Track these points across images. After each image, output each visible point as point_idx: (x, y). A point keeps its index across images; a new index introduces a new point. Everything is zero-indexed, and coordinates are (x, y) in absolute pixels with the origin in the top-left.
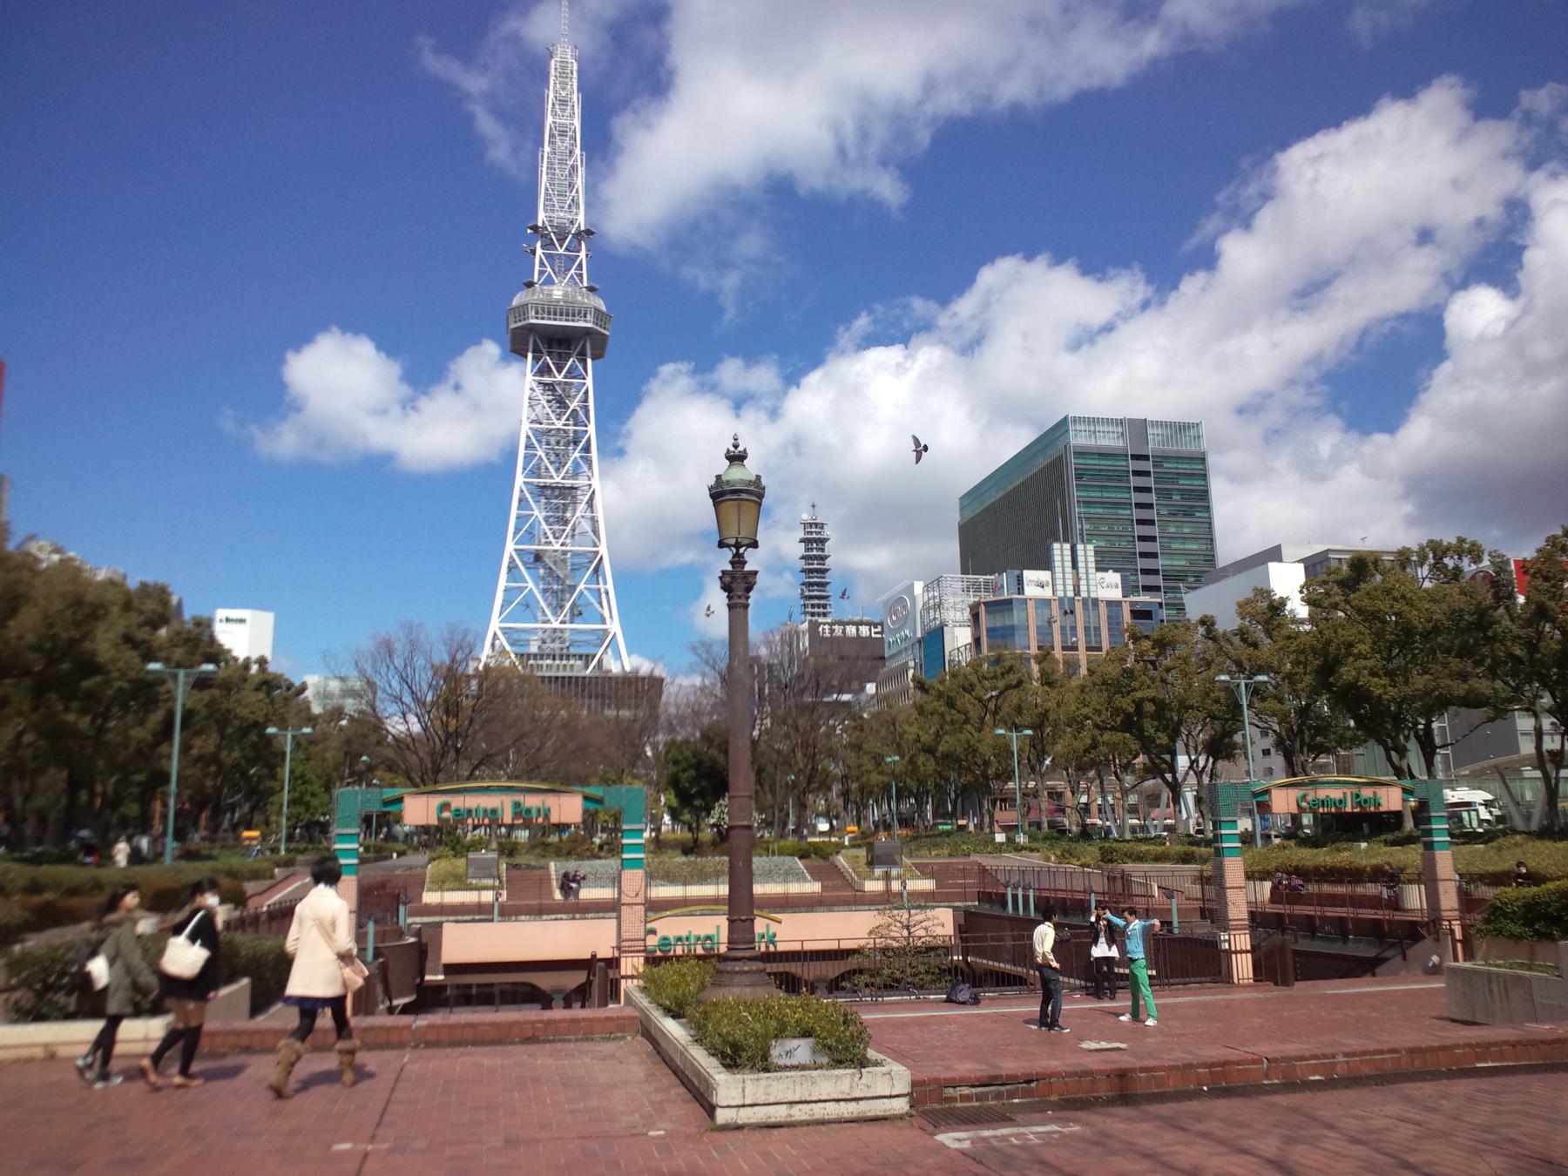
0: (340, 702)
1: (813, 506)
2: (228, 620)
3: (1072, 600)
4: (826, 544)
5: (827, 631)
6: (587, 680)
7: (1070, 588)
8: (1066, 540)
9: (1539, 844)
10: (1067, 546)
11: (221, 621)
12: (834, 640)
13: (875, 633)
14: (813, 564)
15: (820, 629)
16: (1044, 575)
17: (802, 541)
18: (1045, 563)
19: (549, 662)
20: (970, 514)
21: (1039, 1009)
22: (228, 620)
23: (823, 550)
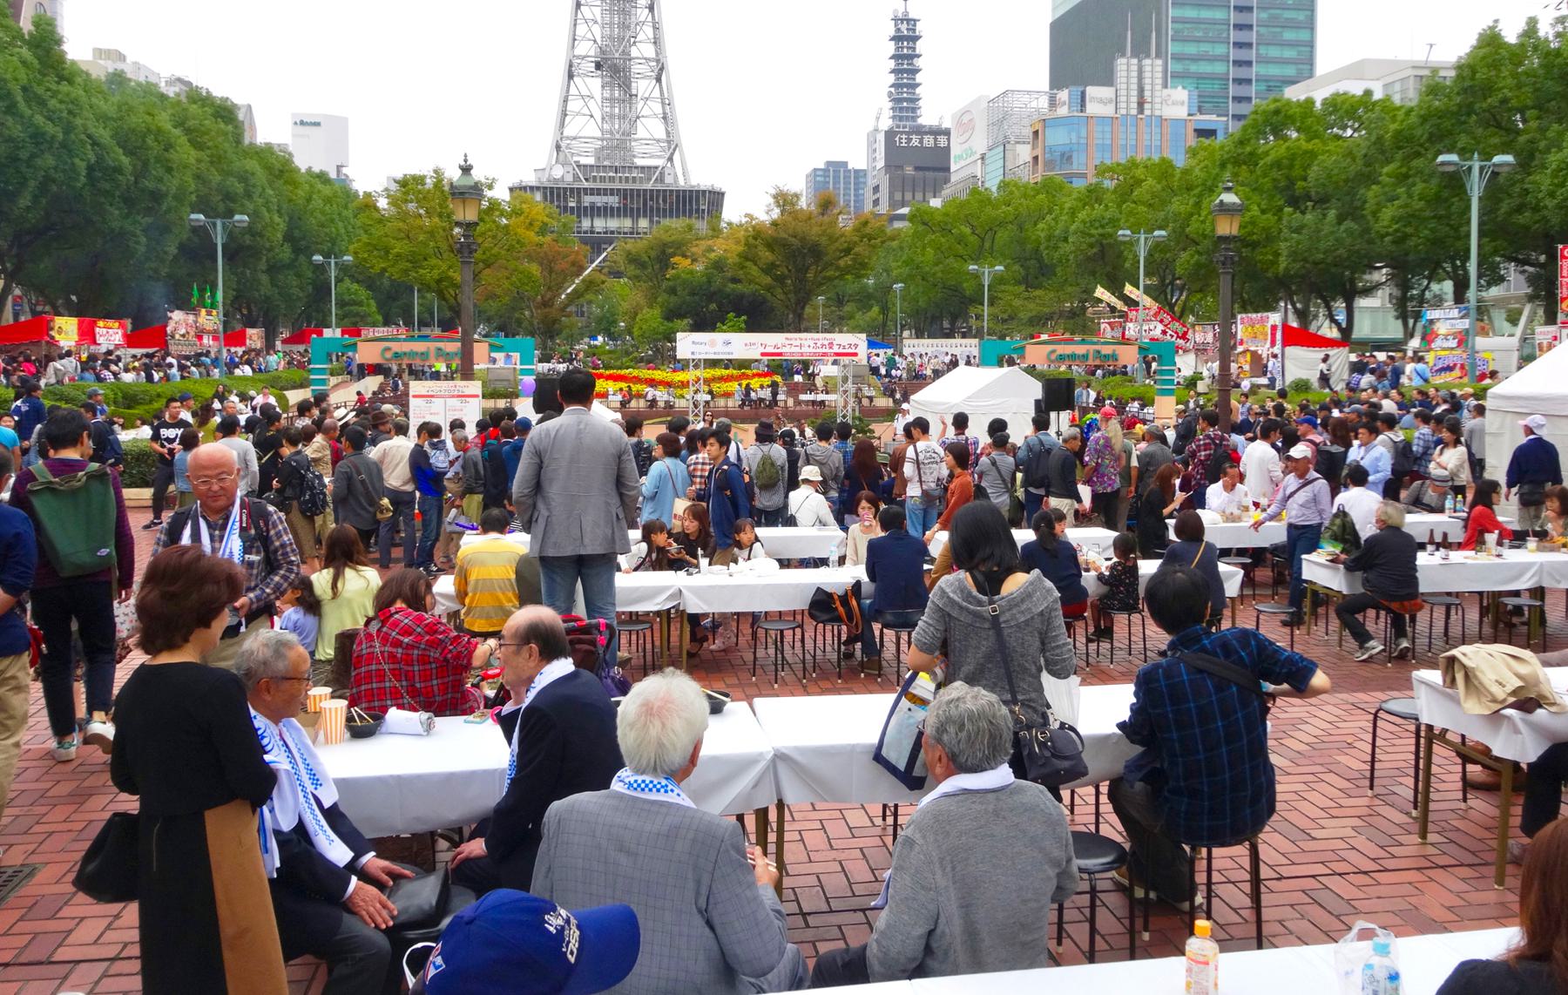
0: (1269, 562)
8: (1158, 56)
10: (1159, 62)
16: (1105, 92)
17: (893, 39)
18: (1108, 79)
20: (276, 149)
21: (476, 367)
23: (914, 49)
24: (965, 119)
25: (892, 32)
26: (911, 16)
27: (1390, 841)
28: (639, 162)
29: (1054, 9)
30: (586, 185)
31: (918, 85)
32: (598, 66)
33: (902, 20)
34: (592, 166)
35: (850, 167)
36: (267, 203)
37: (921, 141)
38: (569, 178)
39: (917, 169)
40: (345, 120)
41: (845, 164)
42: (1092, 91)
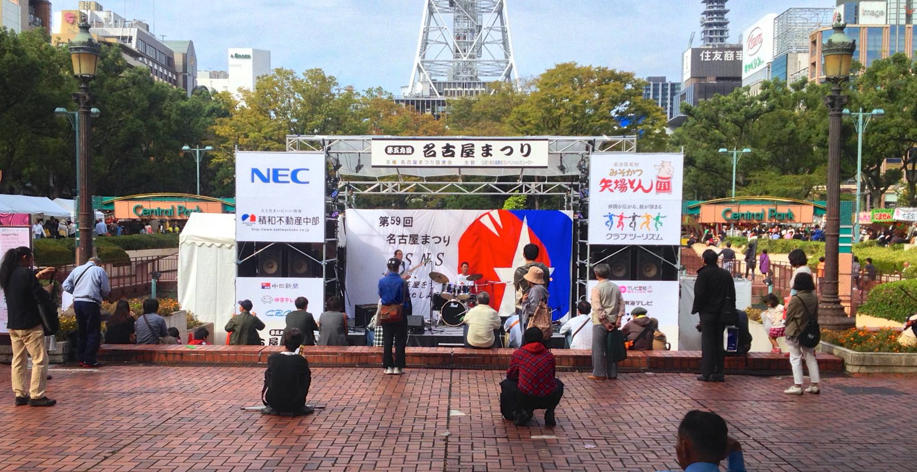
2: (237, 56)
3: (902, 28)
7: (903, 16)
11: (232, 56)
12: (712, 63)
15: (702, 55)
19: (459, 89)
21: (696, 279)
22: (237, 56)
28: (483, 79)
30: (439, 98)
34: (444, 83)
35: (667, 81)
37: (722, 57)
38: (427, 93)
39: (718, 79)
40: (270, 52)
41: (663, 79)
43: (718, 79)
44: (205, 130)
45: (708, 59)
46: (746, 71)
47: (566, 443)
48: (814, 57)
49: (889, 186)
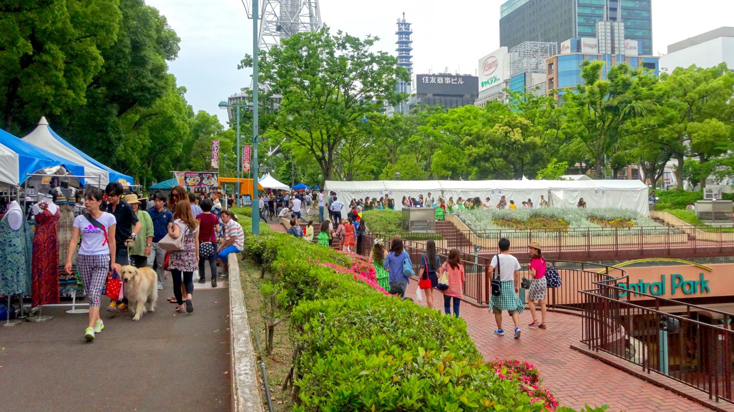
1: (404, 14)
4: (410, 36)
5: (427, 80)
6: (645, 14)
9: (460, 313)
13: (454, 81)
14: (403, 46)
15: (423, 79)
17: (397, 33)
23: (409, 39)
24: (490, 61)
25: (397, 30)
26: (407, 22)
27: (659, 405)
29: (502, 12)
31: (411, 57)
32: (279, 29)
33: (402, 24)
36: (399, 317)
37: (436, 80)
42: (584, 40)
43: (434, 95)
44: (296, 53)
45: (427, 82)
46: (483, 86)
47: (560, 396)
48: (551, 73)
49: (668, 160)
